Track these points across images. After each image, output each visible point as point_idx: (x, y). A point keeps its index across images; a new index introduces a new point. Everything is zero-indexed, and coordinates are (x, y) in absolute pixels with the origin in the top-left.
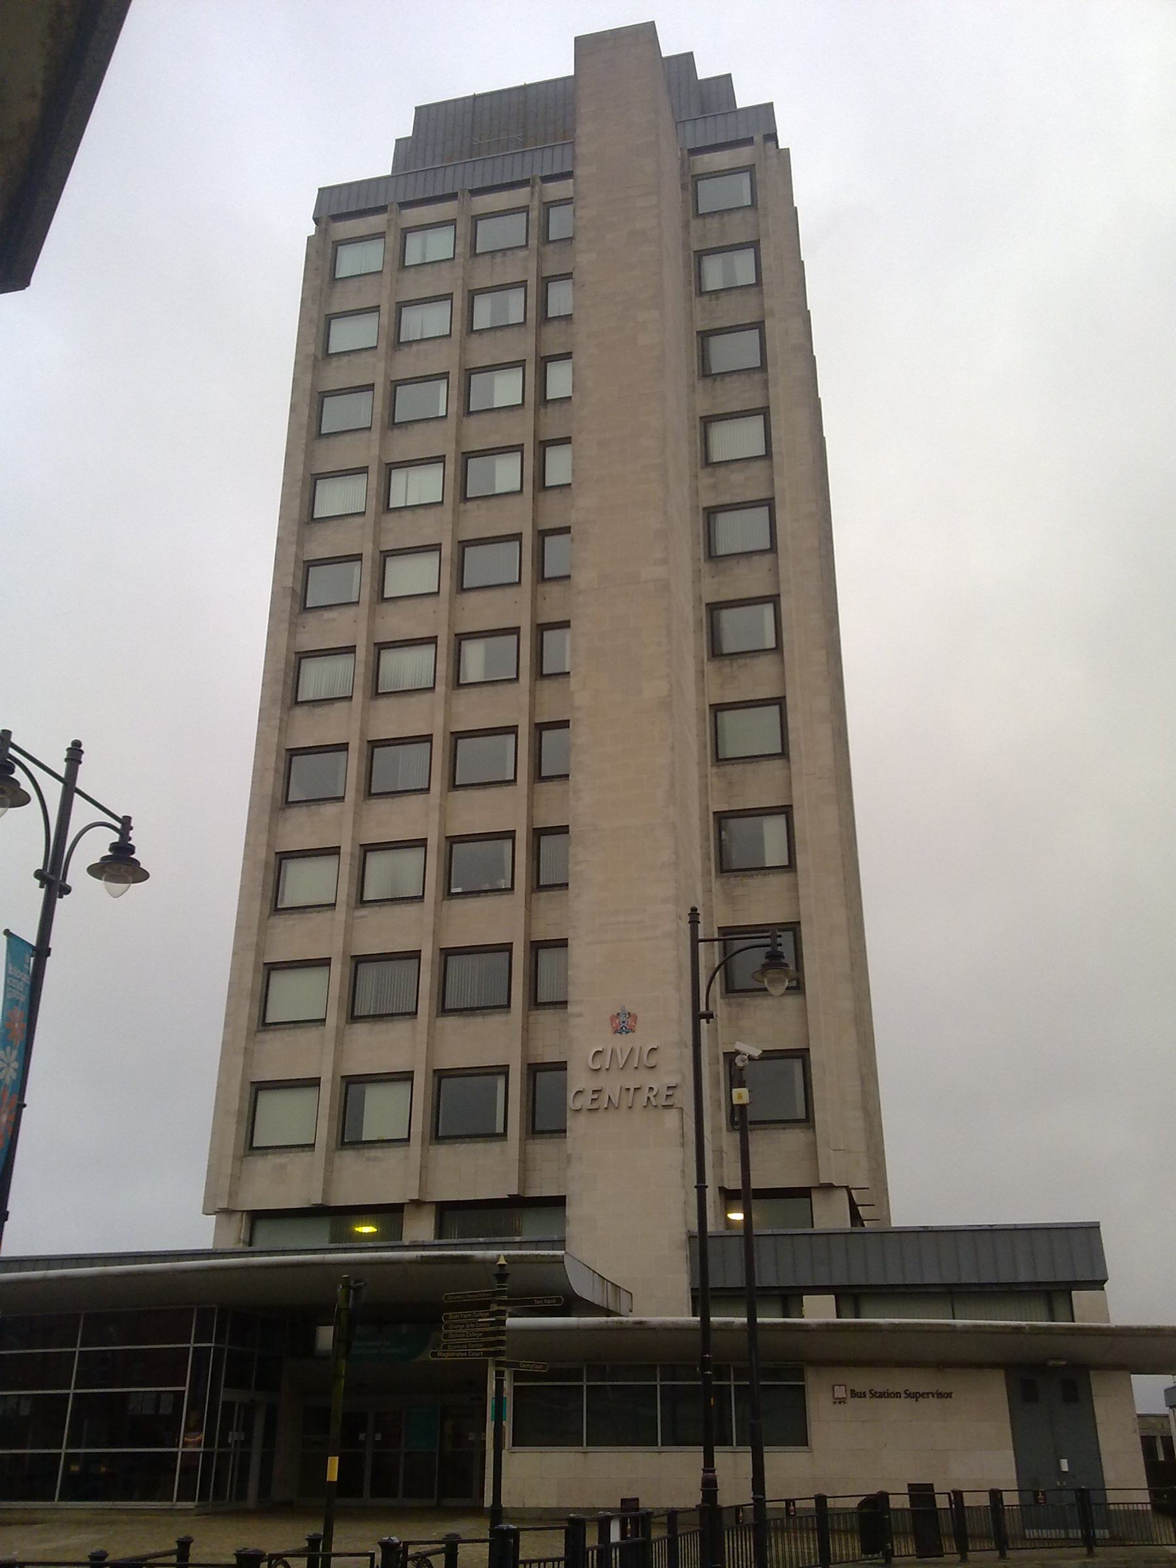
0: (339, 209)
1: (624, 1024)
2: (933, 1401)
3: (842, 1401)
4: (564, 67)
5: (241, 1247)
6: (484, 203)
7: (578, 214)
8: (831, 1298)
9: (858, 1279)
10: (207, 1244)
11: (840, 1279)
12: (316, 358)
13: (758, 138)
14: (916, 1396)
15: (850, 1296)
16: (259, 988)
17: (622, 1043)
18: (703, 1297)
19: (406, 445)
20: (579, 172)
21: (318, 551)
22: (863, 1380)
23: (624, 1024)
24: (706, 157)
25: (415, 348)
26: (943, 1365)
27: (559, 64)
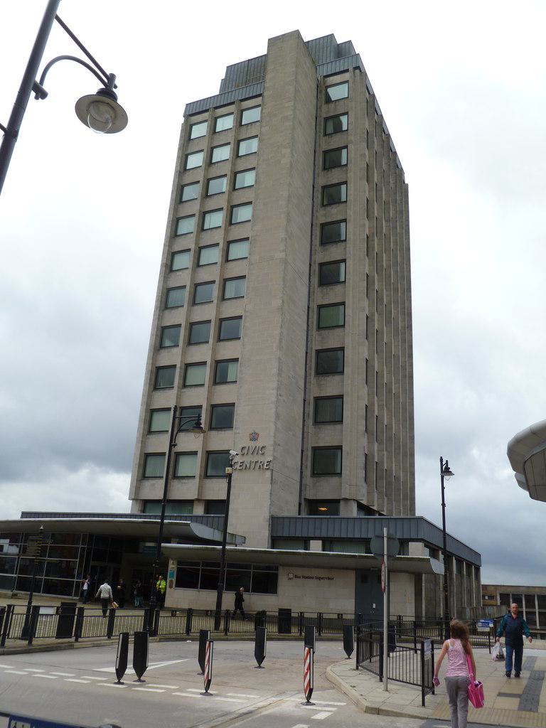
0: (194, 112)
1: (254, 437)
2: (315, 581)
3: (290, 579)
4: (264, 51)
5: (139, 513)
6: (220, 112)
7: (264, 111)
8: (320, 542)
9: (330, 535)
10: (128, 511)
11: (324, 535)
12: (180, 172)
13: (351, 69)
14: (319, 579)
15: (328, 542)
16: (148, 418)
17: (253, 444)
18: (275, 541)
19: (211, 204)
20: (265, 94)
21: (176, 248)
22: (300, 572)
23: (254, 437)
24: (331, 78)
25: (191, 171)
26: (331, 568)
27: (262, 50)
